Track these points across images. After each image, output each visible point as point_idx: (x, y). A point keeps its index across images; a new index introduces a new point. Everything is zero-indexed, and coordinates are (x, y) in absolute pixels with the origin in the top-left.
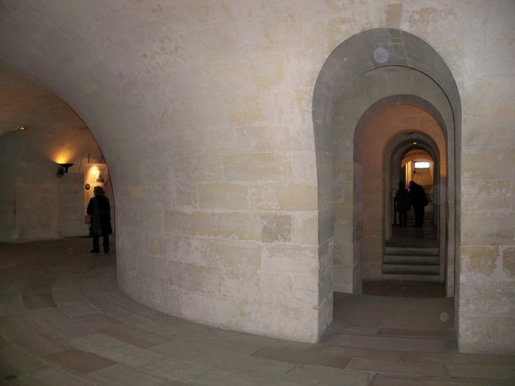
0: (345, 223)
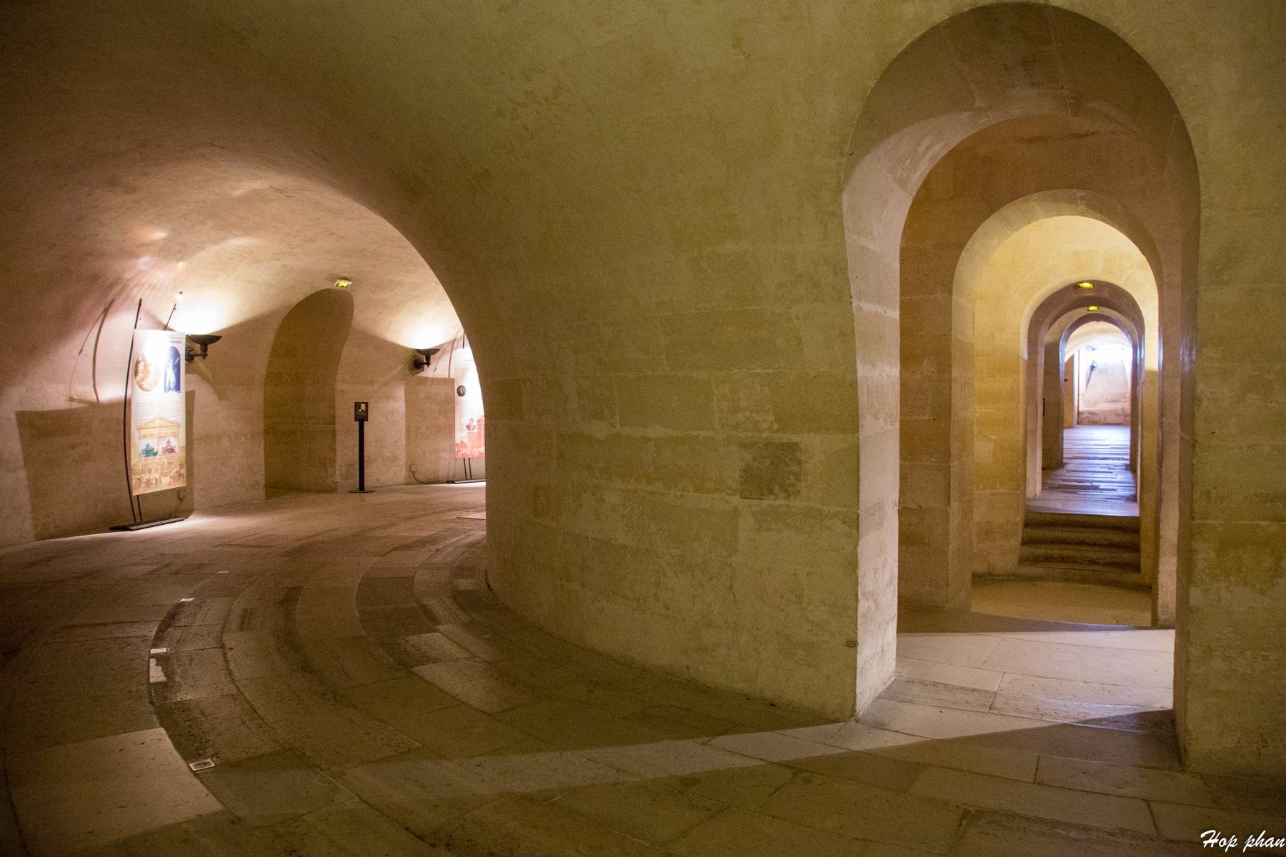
0: (933, 462)
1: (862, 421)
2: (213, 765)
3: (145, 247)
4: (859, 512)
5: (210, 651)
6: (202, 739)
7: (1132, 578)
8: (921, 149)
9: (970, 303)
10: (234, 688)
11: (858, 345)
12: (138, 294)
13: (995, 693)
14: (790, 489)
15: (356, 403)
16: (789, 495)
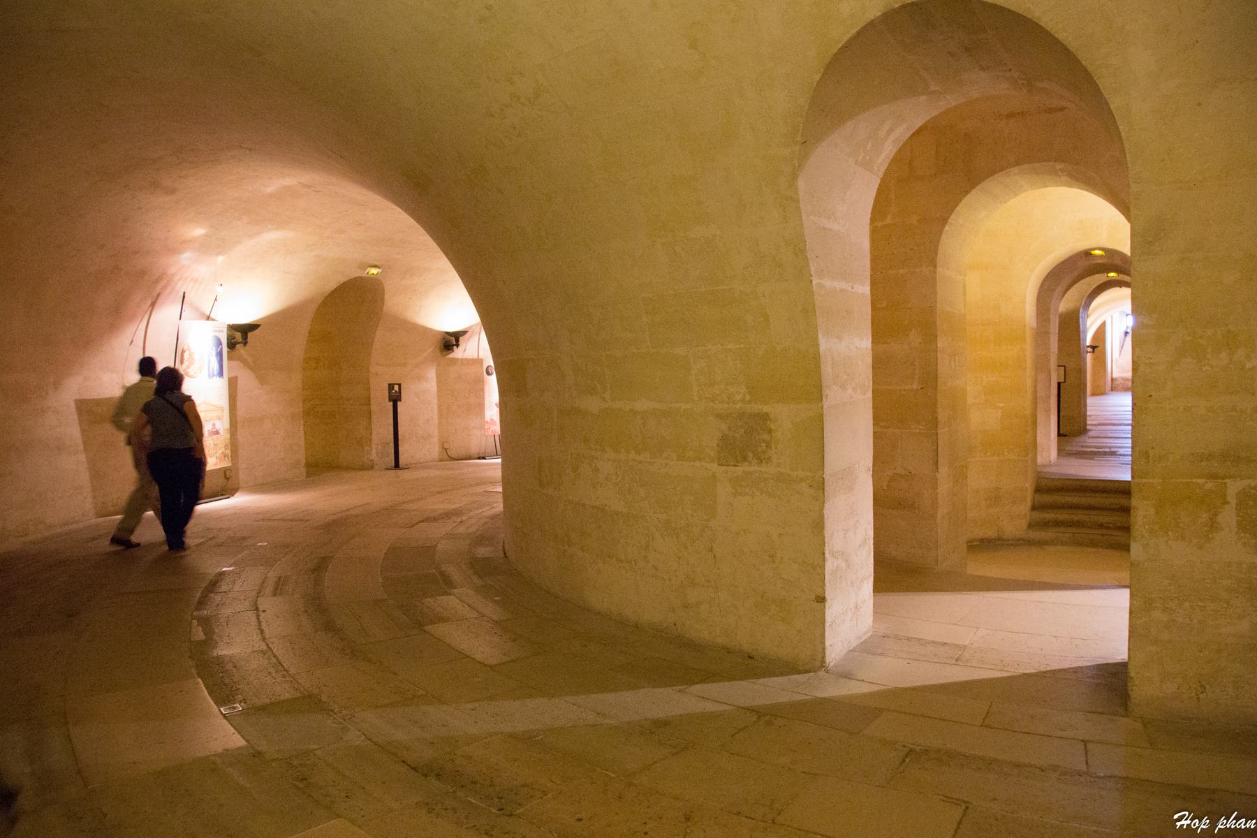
1: (826, 392)
2: (241, 709)
3: (185, 244)
4: (824, 476)
5: (246, 614)
6: (232, 687)
8: (882, 133)
9: (960, 274)
10: (264, 644)
11: (820, 321)
12: (181, 287)
15: (389, 384)
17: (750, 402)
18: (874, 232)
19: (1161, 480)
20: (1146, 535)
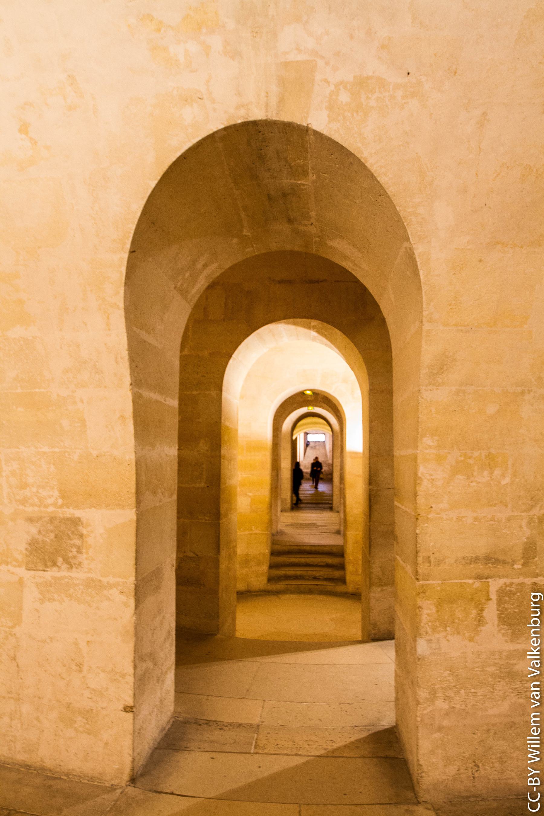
7: (341, 588)
8: (199, 266)
13: (258, 725)
14: (73, 561)
16: (71, 567)
17: (61, 506)
18: (182, 358)
19: (440, 582)
20: (429, 631)
